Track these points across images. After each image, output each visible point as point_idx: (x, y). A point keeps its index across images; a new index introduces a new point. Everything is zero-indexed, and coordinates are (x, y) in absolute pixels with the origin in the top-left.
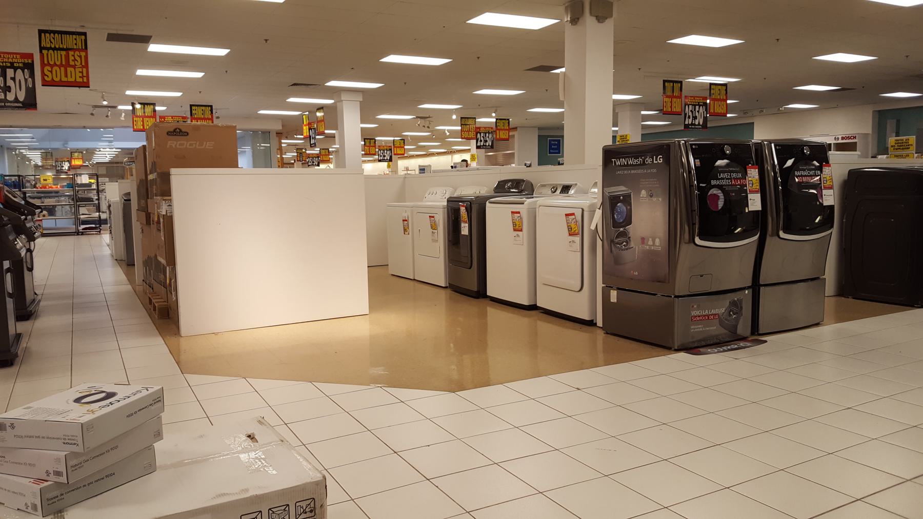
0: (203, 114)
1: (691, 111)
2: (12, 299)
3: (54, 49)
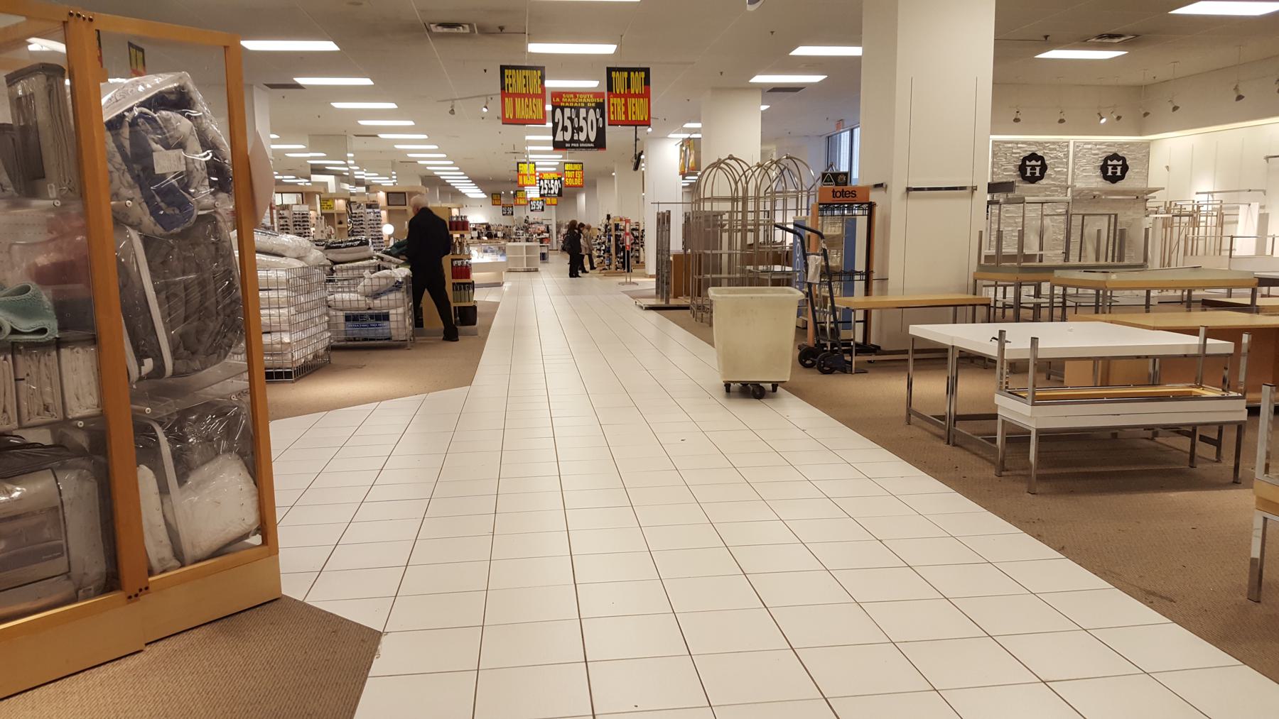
0: (525, 86)
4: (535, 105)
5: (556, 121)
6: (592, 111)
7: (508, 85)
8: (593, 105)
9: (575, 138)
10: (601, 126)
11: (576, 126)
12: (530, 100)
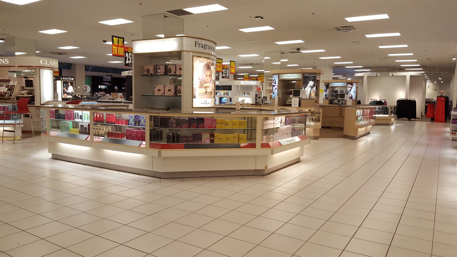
1: (225, 71)
2: (396, 105)
5: (126, 57)
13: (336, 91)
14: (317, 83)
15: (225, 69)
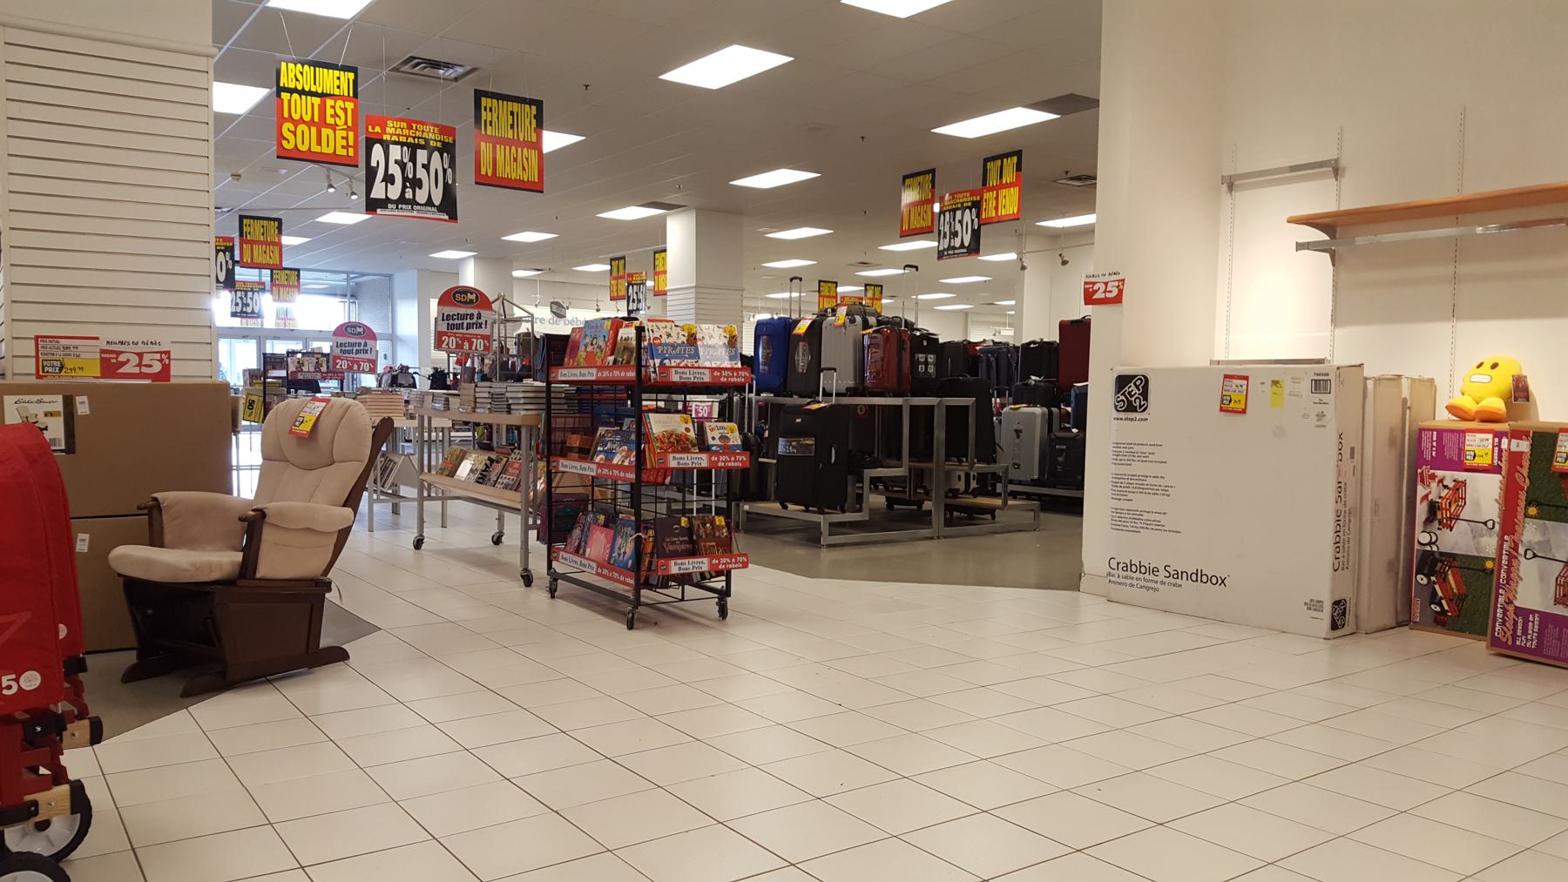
3: (302, 92)
4: (527, 159)
5: (374, 164)
6: (436, 155)
7: (486, 121)
8: (970, 204)
9: (407, 196)
10: (976, 228)
11: (411, 176)
12: (519, 150)
13: (969, 342)
14: (339, 358)
15: (635, 286)
